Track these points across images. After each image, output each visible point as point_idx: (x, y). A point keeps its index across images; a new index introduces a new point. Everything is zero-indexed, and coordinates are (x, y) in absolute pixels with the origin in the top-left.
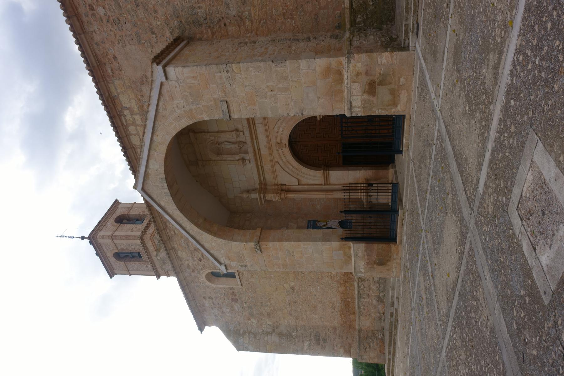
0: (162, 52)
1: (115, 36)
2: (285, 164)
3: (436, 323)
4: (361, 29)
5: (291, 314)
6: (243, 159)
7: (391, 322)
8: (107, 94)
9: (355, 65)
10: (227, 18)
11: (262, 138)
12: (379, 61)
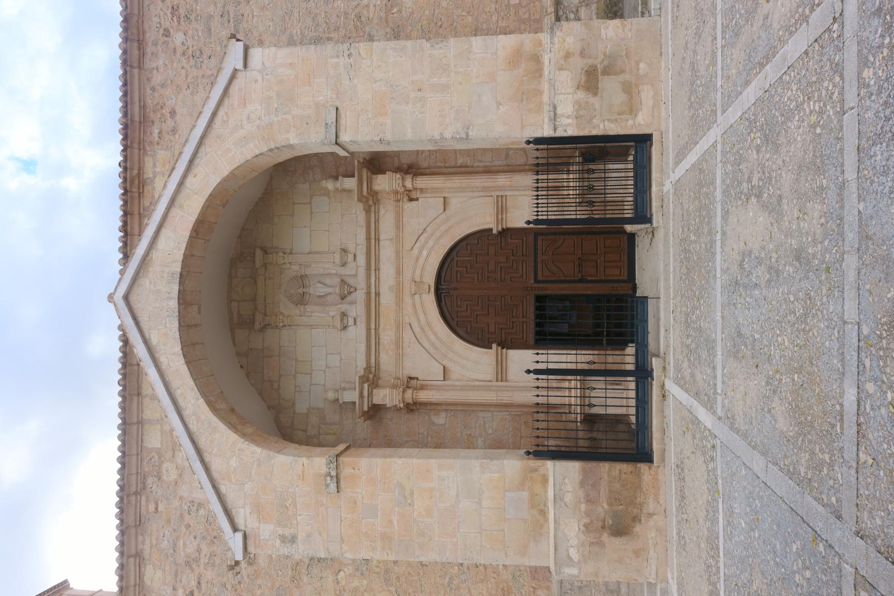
1: (187, 76)
2: (422, 329)
8: (135, 172)
11: (387, 271)
12: (603, 32)
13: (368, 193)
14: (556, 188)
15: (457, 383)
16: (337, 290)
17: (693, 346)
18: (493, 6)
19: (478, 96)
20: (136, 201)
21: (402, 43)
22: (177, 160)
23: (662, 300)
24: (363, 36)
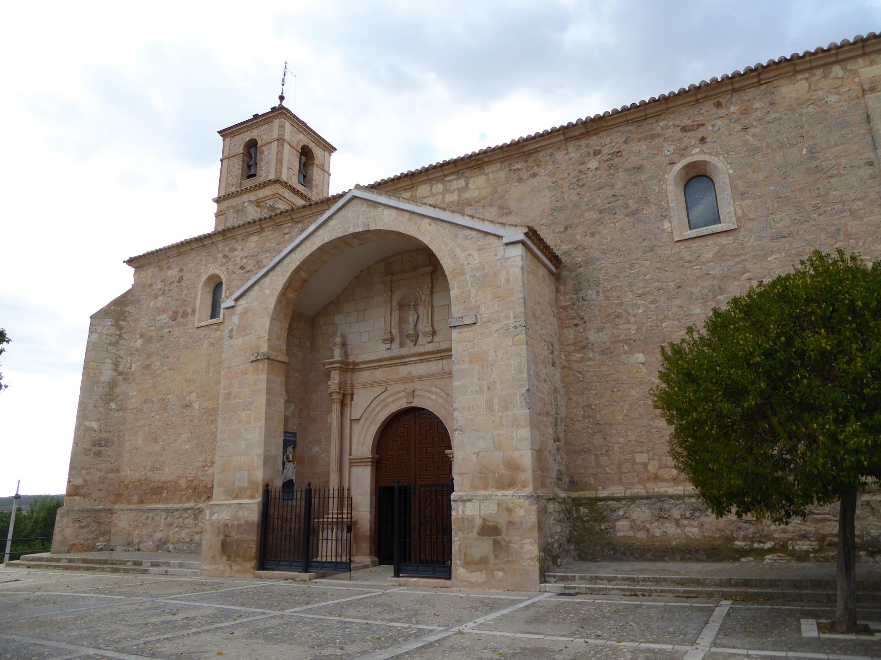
0: (541, 240)
1: (563, 179)
2: (383, 400)
3: (139, 637)
4: (569, 513)
5: (145, 402)
6: (392, 340)
7: (124, 563)
8: (486, 160)
9: (521, 505)
10: (585, 329)
11: (421, 369)
12: (528, 541)
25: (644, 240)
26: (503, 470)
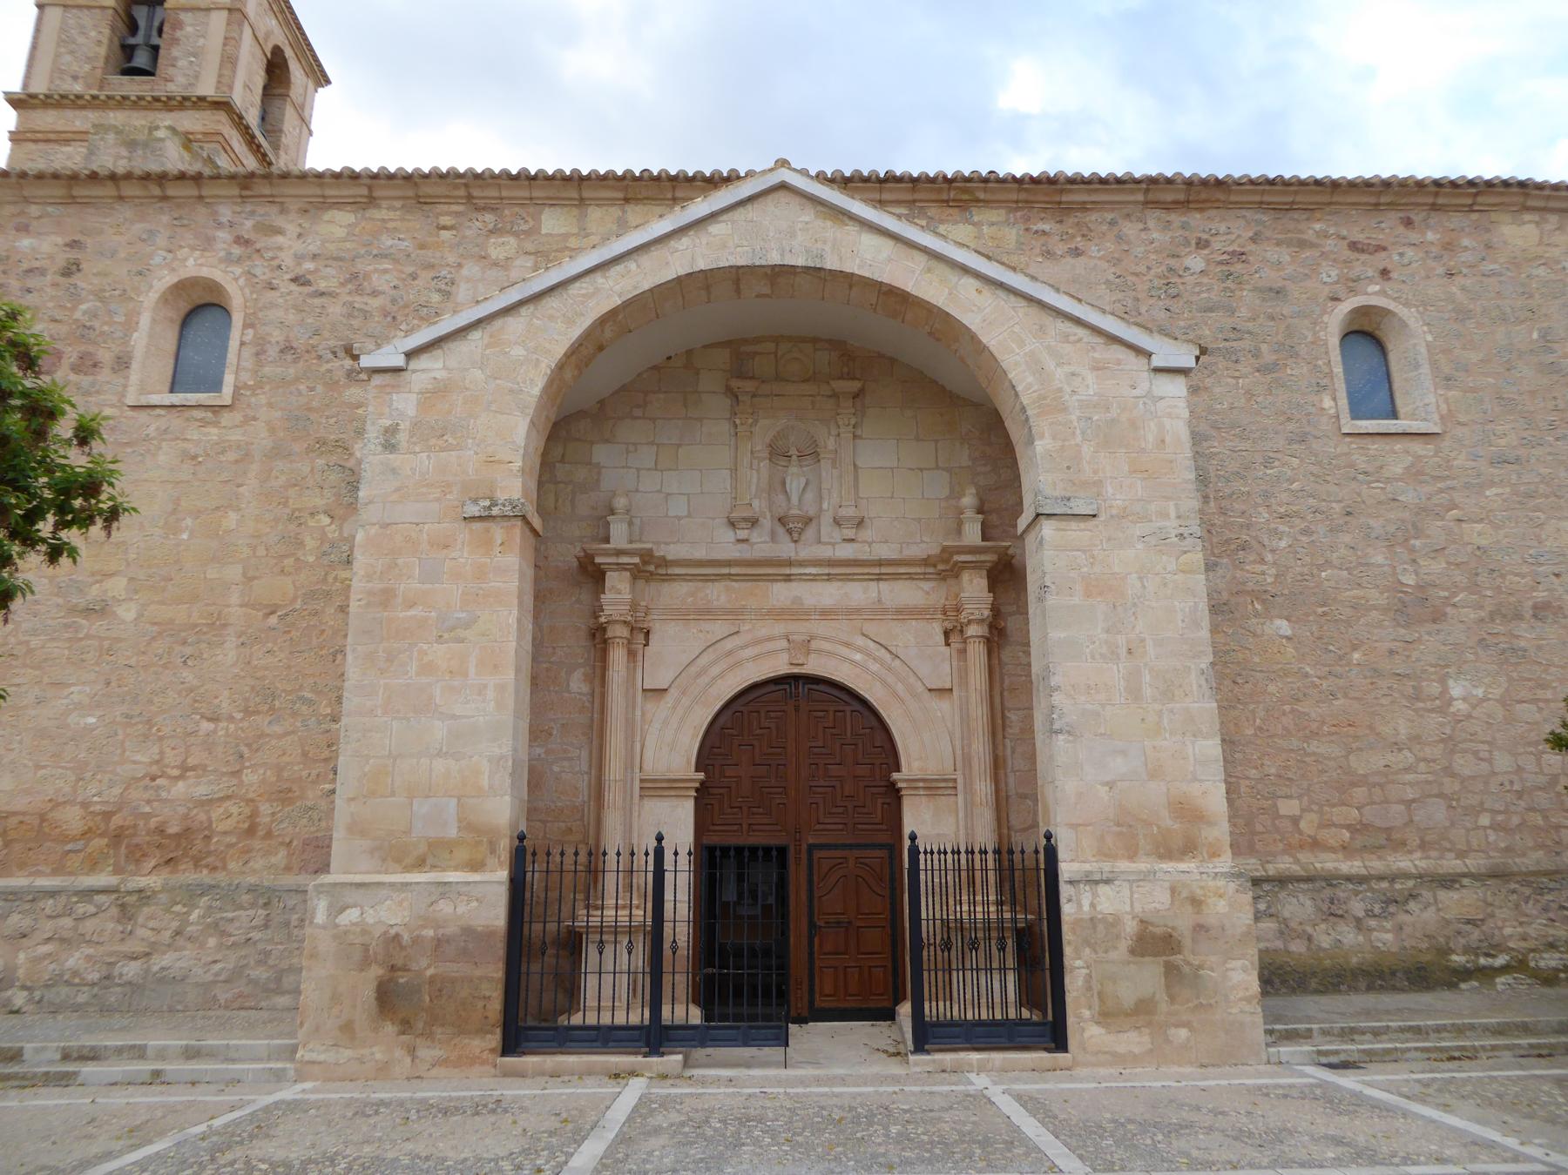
1: (1136, 274)
2: (730, 653)
8: (982, 196)
11: (828, 594)
12: (1238, 964)
13: (956, 563)
14: (972, 882)
15: (638, 713)
16: (795, 512)
17: (710, 1132)
18: (1273, 771)
19: (1126, 747)
20: (933, 197)
21: (1206, 623)
22: (1003, 264)
23: (782, 1072)
24: (1213, 554)
25: (1289, 419)
26: (1168, 822)
